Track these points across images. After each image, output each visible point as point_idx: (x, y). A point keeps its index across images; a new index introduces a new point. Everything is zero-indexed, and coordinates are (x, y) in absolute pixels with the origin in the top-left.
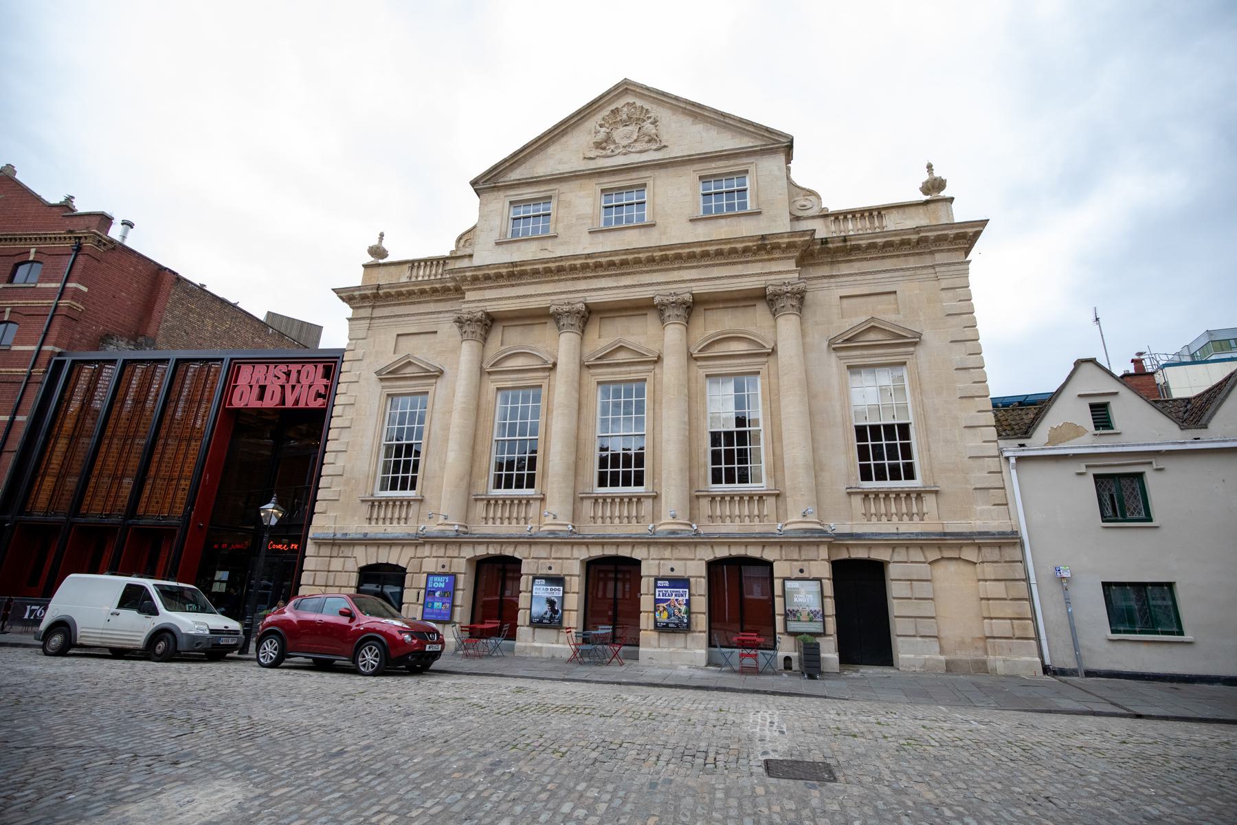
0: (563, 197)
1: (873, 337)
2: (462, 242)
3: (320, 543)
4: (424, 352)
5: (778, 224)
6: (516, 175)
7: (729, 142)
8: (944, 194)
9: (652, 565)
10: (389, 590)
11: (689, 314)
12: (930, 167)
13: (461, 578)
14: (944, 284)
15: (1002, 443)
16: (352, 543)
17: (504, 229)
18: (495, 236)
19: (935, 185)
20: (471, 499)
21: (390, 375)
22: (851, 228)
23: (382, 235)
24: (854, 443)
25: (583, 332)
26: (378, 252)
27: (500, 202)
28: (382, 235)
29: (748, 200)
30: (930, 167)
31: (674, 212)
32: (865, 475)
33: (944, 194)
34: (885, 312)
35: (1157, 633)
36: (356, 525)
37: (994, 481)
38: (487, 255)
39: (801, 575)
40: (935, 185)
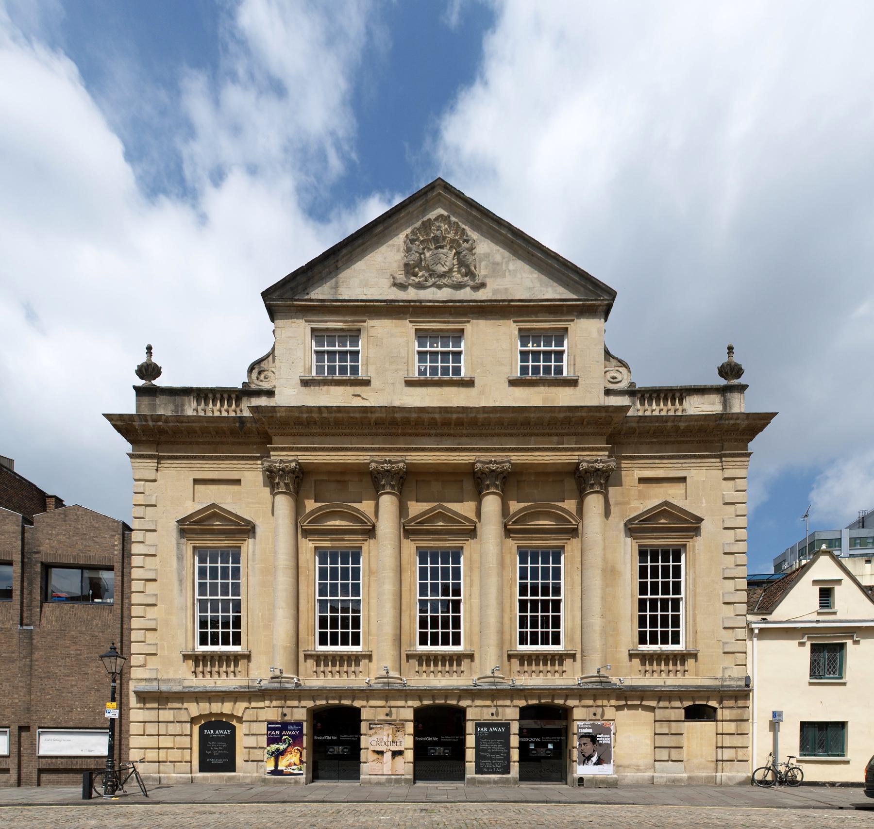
0: (372, 332)
1: (440, 524)
2: (255, 372)
3: (143, 697)
4: (229, 500)
5: (589, 395)
6: (320, 293)
7: (552, 291)
8: (742, 381)
9: (476, 712)
10: (741, 703)
11: (402, 485)
12: (730, 349)
13: (305, 724)
14: (728, 473)
15: (750, 618)
16: (181, 697)
17: (308, 366)
18: (300, 372)
19: (731, 371)
20: (297, 655)
21: (188, 527)
22: (191, 409)
23: (149, 348)
24: (243, 630)
25: (297, 493)
26: (149, 371)
27: (298, 331)
28: (149, 348)
29: (462, 364)
30: (730, 349)
31: (491, 366)
32: (642, 640)
33: (742, 381)
34: (674, 495)
35: (829, 755)
36: (184, 677)
37: (738, 647)
38: (289, 395)
39: (594, 718)
40: (731, 371)
